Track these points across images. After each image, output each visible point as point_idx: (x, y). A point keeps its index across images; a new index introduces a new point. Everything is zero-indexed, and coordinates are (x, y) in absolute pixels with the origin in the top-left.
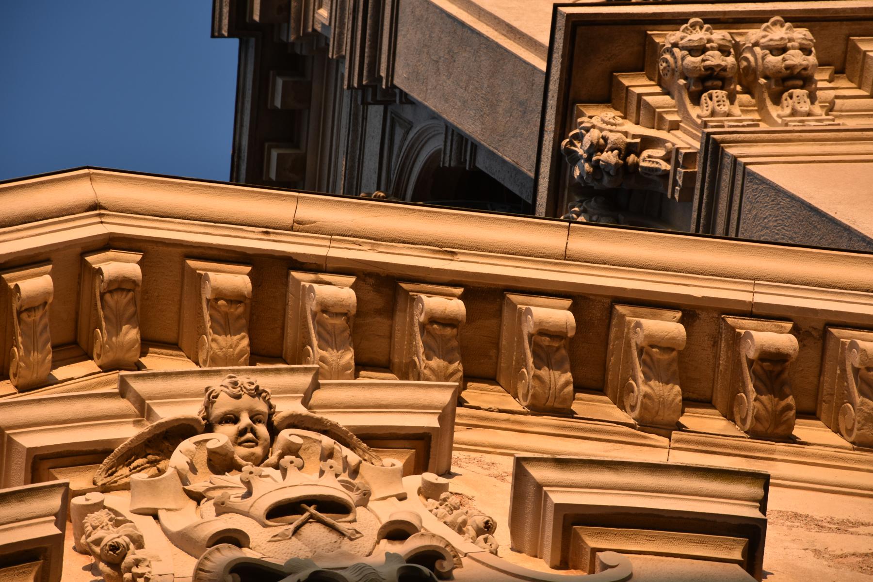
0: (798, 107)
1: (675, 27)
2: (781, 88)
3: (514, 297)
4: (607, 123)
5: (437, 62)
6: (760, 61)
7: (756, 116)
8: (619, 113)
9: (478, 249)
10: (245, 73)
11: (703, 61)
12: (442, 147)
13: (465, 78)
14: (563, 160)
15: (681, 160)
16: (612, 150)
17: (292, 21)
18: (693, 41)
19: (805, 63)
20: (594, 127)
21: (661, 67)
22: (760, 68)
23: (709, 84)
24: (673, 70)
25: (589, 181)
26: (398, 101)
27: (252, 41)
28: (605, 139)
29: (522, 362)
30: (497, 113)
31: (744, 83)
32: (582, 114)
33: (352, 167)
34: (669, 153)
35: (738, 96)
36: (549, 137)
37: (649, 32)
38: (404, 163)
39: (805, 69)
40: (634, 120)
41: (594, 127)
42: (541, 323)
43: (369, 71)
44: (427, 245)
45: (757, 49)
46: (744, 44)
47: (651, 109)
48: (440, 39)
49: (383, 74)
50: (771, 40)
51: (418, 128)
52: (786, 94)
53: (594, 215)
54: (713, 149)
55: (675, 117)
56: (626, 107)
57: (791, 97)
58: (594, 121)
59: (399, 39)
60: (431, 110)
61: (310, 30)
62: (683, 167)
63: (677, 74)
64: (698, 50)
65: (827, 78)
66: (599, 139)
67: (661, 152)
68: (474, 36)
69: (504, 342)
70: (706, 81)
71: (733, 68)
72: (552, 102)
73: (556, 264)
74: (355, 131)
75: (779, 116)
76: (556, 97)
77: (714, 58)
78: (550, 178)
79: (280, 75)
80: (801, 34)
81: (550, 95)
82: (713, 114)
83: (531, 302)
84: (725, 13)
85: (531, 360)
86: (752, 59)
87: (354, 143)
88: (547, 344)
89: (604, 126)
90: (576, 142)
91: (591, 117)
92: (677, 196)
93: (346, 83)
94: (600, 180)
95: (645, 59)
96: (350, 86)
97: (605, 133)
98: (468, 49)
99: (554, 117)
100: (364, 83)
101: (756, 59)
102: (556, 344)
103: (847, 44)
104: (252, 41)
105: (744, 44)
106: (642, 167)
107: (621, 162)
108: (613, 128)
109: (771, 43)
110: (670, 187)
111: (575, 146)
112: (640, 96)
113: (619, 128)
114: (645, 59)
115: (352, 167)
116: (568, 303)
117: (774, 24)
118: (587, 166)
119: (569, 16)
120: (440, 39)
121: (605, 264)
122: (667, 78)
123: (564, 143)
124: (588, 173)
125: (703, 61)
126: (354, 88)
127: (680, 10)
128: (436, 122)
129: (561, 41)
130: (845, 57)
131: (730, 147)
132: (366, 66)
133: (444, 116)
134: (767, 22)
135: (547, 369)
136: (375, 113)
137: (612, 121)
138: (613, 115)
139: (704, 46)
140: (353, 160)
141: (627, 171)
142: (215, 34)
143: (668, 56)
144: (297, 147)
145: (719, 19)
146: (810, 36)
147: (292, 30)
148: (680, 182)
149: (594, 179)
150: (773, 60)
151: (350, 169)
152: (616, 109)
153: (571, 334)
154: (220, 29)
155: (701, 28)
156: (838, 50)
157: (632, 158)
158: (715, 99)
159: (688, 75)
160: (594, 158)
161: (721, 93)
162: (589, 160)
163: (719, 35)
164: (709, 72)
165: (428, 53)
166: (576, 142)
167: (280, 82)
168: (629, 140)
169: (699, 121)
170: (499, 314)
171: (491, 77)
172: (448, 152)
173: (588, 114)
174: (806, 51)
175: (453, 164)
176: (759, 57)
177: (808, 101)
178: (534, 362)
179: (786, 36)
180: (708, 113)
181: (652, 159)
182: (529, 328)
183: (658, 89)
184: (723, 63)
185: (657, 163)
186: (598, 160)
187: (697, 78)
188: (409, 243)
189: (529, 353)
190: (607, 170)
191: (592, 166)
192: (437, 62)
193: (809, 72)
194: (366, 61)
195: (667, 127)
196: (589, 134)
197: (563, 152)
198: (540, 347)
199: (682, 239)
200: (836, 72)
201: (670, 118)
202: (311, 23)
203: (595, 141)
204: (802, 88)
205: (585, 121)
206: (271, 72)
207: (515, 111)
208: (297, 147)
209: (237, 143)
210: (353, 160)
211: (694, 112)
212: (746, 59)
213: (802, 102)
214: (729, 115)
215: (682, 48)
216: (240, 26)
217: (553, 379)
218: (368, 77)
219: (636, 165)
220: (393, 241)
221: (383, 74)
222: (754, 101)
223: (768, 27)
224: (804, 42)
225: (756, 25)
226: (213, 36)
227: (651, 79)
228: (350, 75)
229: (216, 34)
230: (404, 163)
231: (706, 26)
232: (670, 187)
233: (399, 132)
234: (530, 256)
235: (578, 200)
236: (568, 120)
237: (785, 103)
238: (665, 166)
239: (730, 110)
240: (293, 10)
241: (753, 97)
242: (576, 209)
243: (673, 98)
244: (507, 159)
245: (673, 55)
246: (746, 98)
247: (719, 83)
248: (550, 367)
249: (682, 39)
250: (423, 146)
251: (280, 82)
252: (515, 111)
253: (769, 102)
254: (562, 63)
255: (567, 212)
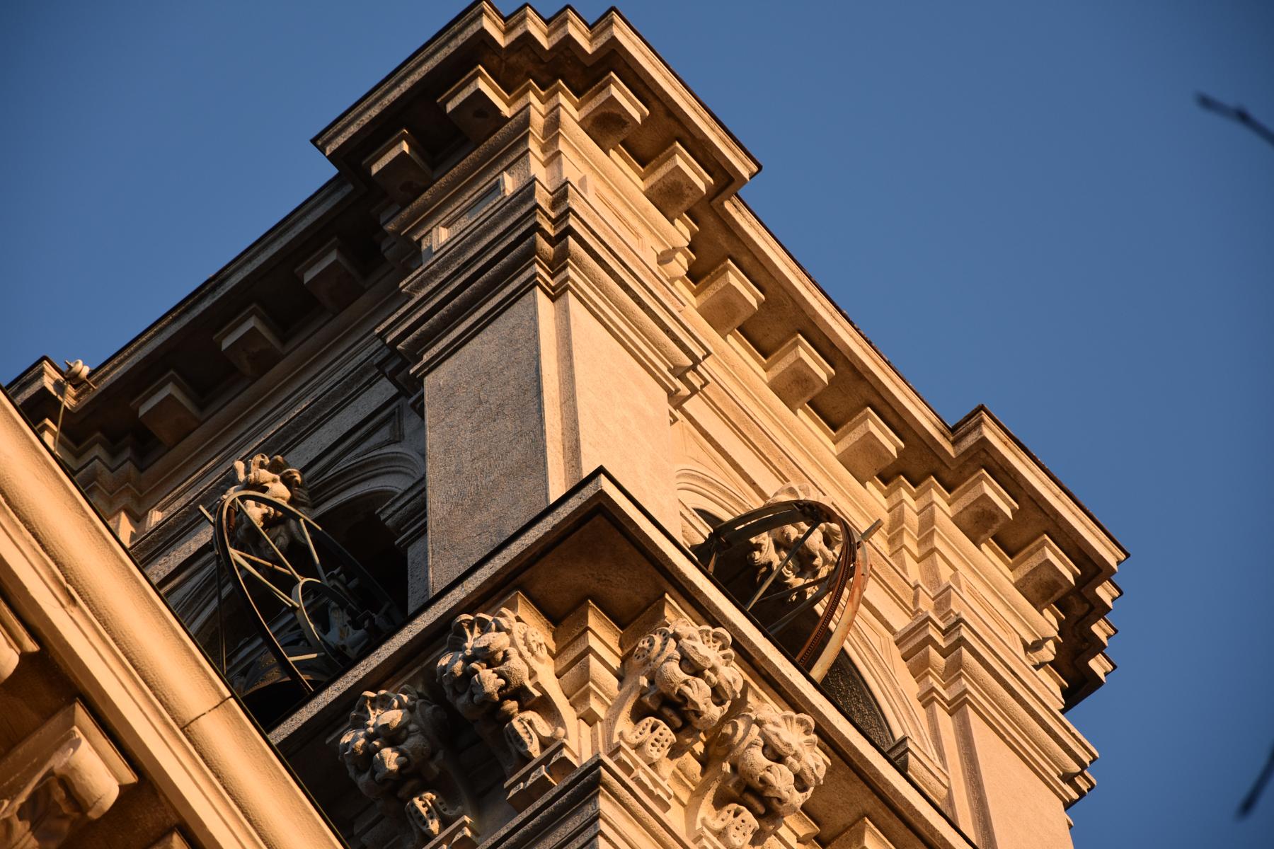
0: (732, 832)
1: (699, 618)
2: (737, 794)
3: (81, 713)
4: (527, 643)
5: (481, 403)
6: (745, 744)
7: (685, 797)
8: (552, 646)
9: (104, 623)
10: (308, 212)
11: (686, 683)
12: (400, 492)
13: (485, 448)
14: (446, 633)
15: (554, 760)
16: (500, 676)
17: (408, 210)
18: (697, 652)
19: (785, 794)
20: (509, 632)
21: (641, 645)
22: (738, 752)
23: (668, 712)
24: (648, 660)
25: (446, 683)
26: (411, 401)
27: (349, 188)
28: (506, 657)
29: (12, 793)
30: (473, 517)
31: (711, 750)
32: (513, 607)
33: (307, 419)
34: (552, 739)
35: (688, 755)
36: (458, 594)
37: (667, 596)
38: (352, 471)
39: (780, 801)
40: (559, 668)
41: (509, 632)
42: (74, 770)
43: (416, 340)
44: (56, 564)
45: (755, 729)
46: (751, 711)
47: (585, 677)
48: (507, 383)
49: (426, 358)
50: (777, 735)
51: (400, 450)
52: (734, 806)
53: (416, 723)
54: (588, 783)
55: (600, 711)
56: (565, 648)
57: (736, 815)
58: (517, 628)
59: (476, 340)
60: (424, 443)
61: (416, 238)
62: (549, 771)
63: (648, 668)
64: (694, 668)
65: (801, 835)
66: (499, 650)
67: (545, 729)
68: (536, 416)
69: (20, 751)
70: (665, 706)
71: (708, 721)
72: (498, 563)
73: (167, 724)
74: (348, 386)
75: (703, 820)
76: (506, 561)
77: (699, 692)
78: (415, 638)
79: (341, 250)
80: (815, 761)
81: (505, 553)
82: (638, 747)
83: (93, 738)
84: (765, 658)
85: (22, 799)
86: (740, 733)
87: (334, 397)
88: (57, 799)
89: (520, 642)
90: (476, 629)
91: (518, 619)
92: (513, 792)
93: (382, 327)
94: (457, 694)
95: (635, 619)
96: (382, 336)
97: (512, 651)
98: (518, 422)
99: (484, 579)
100: (399, 347)
101: (743, 738)
102: (65, 809)
103: (857, 821)
104: (349, 188)
105: (751, 711)
106: (512, 726)
107: (497, 697)
108: (527, 655)
109: (774, 738)
110: (517, 776)
111: (472, 632)
112: (589, 650)
113: (532, 661)
114: (635, 619)
115: (307, 419)
116: (130, 777)
117: (801, 722)
118: (459, 665)
119: (602, 494)
120: (507, 383)
121: (218, 777)
122: (635, 661)
123: (464, 617)
124: (452, 673)
125: (686, 683)
126: (384, 340)
127: (721, 607)
128: (418, 457)
129: (569, 510)
130: (842, 833)
131: (608, 798)
132: (418, 332)
133: (429, 465)
134: (797, 712)
135: (28, 826)
136: (384, 390)
137: (534, 646)
138: (542, 641)
139: (704, 669)
140: (314, 414)
141: (493, 713)
142: (318, 141)
143: (658, 640)
144: (284, 341)
145: (752, 658)
146: (821, 773)
147: (397, 219)
148: (529, 783)
149: (453, 686)
150: (757, 758)
151: (303, 418)
152: (555, 639)
153: (93, 815)
154: (328, 142)
155: (723, 648)
156: (841, 818)
157: (512, 705)
158: (657, 732)
159: (658, 683)
160: (474, 665)
161: (669, 735)
162: (468, 660)
163: (732, 675)
164: (679, 700)
165: (482, 384)
166: (476, 629)
167: (333, 257)
168: (529, 684)
169: (616, 739)
170: (48, 715)
171: (504, 475)
172: (398, 505)
173: (519, 613)
174: (800, 782)
175: (388, 523)
176: (749, 739)
177: (750, 837)
178: (22, 806)
179: (795, 746)
180: (635, 741)
181: (531, 728)
182: (57, 763)
183: (616, 663)
184: (702, 707)
185: (531, 737)
186: (476, 672)
187: (662, 694)
188: (39, 541)
189: (29, 790)
190: (475, 690)
191: (464, 670)
192: (481, 403)
193: (782, 808)
194: (424, 327)
195: (582, 711)
196: (495, 634)
197: (453, 625)
198: (49, 795)
199: (326, 835)
200: (817, 838)
201: (595, 705)
202: (423, 232)
203: (493, 648)
204: (758, 816)
205: (508, 617)
206: (335, 239)
207: (487, 535)
208: (284, 341)
209: (227, 272)
210: (314, 414)
211: (624, 724)
212: (735, 728)
213: (741, 832)
214: (653, 765)
215: (679, 648)
216: (350, 160)
217: (22, 843)
218: (409, 345)
219: (510, 717)
220: (25, 521)
221: (426, 358)
222: (699, 778)
223: (791, 718)
224: (808, 772)
225: (784, 704)
226: (314, 141)
227: (621, 646)
228: (393, 326)
229: (319, 143)
230: (352, 471)
231: (730, 651)
232: (517, 776)
233: (384, 434)
234: (150, 687)
235: (420, 690)
236: (495, 598)
237: (724, 813)
238: (534, 749)
239: (659, 760)
240: (420, 200)
241: (703, 774)
242: (405, 698)
243: (620, 688)
244: (431, 575)
245: (664, 644)
246: (695, 767)
247: (679, 723)
248: (34, 828)
249: (689, 638)
250: (388, 473)
251: (333, 257)
252: (487, 535)
253: (710, 796)
254: (547, 534)
255: (395, 692)
